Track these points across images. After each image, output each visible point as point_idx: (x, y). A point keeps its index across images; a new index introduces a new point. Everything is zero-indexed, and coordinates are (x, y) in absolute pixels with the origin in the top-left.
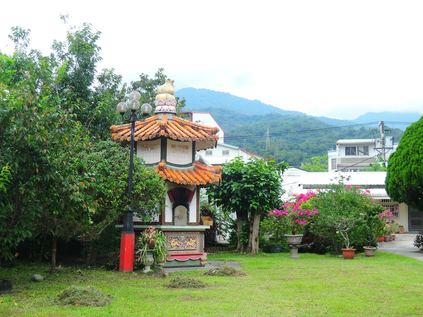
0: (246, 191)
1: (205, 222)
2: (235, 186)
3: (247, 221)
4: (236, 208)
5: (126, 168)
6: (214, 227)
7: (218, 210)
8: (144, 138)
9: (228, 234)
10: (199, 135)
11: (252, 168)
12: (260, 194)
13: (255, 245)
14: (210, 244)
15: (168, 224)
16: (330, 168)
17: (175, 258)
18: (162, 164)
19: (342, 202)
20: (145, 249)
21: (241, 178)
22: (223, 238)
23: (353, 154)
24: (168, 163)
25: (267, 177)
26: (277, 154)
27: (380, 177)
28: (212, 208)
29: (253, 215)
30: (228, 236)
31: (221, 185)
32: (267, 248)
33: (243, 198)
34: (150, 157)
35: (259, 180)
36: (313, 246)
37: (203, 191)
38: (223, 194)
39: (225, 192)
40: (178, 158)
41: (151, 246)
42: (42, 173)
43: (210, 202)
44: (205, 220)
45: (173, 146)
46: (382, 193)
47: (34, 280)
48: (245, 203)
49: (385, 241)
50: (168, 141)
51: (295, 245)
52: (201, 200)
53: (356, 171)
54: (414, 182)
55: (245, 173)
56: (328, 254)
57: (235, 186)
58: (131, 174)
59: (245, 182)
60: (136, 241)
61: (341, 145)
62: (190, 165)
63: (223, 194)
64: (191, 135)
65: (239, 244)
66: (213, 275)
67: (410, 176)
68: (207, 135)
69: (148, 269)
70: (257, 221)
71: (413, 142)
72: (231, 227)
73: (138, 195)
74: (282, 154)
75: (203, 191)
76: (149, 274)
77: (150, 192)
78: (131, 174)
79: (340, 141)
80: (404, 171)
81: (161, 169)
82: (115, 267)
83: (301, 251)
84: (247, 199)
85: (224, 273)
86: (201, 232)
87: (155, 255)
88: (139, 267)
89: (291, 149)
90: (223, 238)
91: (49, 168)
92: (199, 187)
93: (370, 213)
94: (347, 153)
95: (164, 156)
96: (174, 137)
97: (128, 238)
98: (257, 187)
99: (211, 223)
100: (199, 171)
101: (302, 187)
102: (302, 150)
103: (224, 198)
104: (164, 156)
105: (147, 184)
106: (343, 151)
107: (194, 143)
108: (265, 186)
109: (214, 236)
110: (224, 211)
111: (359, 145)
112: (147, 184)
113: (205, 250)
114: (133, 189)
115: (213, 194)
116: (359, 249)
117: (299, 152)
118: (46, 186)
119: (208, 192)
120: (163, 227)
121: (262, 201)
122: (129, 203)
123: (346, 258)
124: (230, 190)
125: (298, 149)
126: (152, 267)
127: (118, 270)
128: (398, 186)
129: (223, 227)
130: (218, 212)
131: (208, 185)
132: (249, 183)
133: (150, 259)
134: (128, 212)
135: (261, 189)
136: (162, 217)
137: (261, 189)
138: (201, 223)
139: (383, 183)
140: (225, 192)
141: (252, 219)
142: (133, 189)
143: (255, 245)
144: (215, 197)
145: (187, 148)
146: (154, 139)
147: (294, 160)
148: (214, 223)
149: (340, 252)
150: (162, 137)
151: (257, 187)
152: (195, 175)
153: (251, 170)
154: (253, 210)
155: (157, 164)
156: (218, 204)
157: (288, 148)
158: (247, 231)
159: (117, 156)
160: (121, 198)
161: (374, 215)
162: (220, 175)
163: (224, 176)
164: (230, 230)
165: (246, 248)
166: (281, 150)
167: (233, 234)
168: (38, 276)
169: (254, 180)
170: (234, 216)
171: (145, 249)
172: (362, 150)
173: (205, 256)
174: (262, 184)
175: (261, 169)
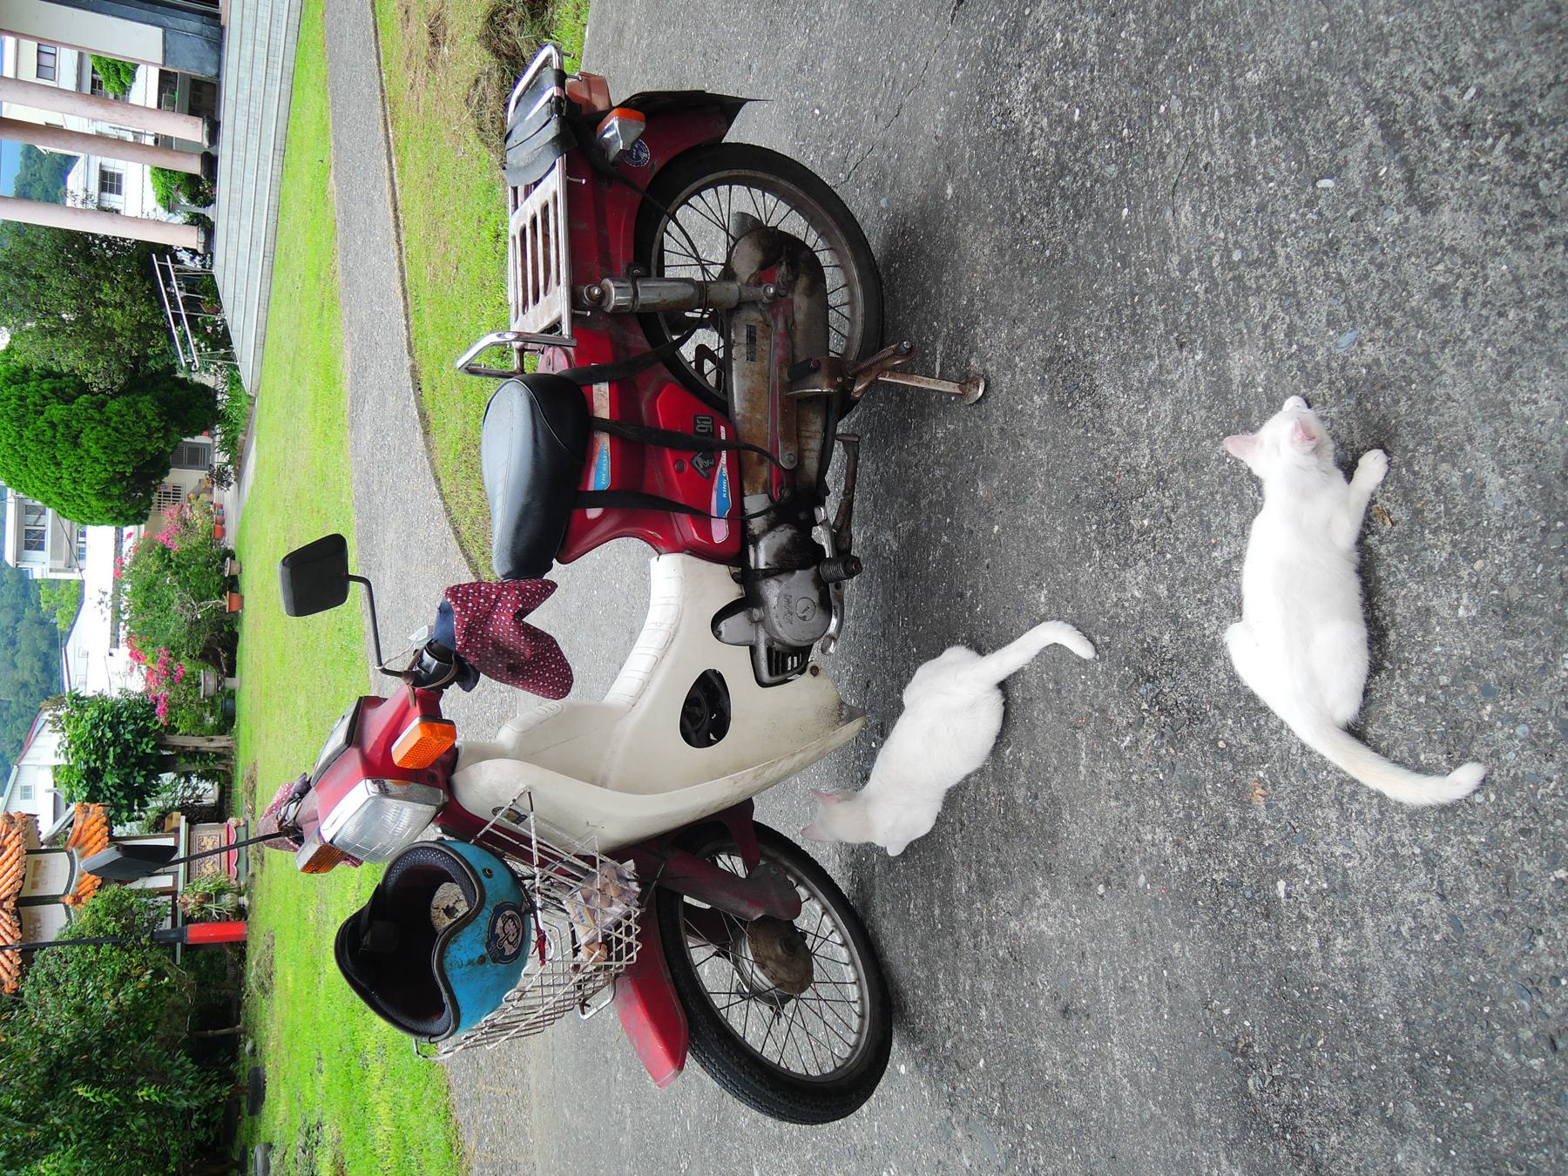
0: (120, 760)
1: (174, 825)
2: (111, 779)
3: (178, 755)
4: (153, 775)
5: (77, 950)
6: (184, 809)
7: (155, 804)
8: (18, 935)
9: (201, 785)
10: (15, 844)
11: (77, 752)
12: (128, 736)
13: (220, 742)
14: (219, 813)
15: (175, 881)
16: (74, 576)
17: (233, 865)
18: (68, 900)
19: (146, 605)
20: (212, 907)
21: (96, 769)
22: (209, 792)
23: (42, 535)
24: (67, 891)
25: (95, 726)
26: (26, 676)
27: (100, 538)
28: (151, 814)
29: (166, 748)
30: (204, 785)
31: (107, 802)
32: (228, 721)
33: (134, 765)
34: (54, 922)
35: (100, 739)
36: (225, 649)
37: (118, 831)
38: (124, 797)
39: (121, 794)
40: (57, 874)
41: (208, 898)
42: (89, 1049)
43: (140, 818)
44: (169, 824)
45: (34, 885)
46: (134, 533)
47: (253, 1050)
48: (143, 761)
49: (223, 522)
50: (23, 894)
51: (219, 683)
52: (136, 832)
53: (82, 550)
54: (115, 491)
55: (87, 762)
56: (237, 629)
57: (111, 779)
58: (89, 942)
59: (103, 763)
60: (200, 920)
61: (18, 558)
62: (70, 855)
63: (124, 797)
64: (15, 856)
65: (220, 768)
66: (254, 808)
67: (103, 495)
68: (14, 832)
69: (244, 900)
70: (177, 740)
71: (38, 484)
72: (188, 780)
73: (124, 927)
74: (27, 665)
75: (118, 831)
76: (250, 897)
77: (119, 909)
78: (89, 942)
79: (9, 557)
80: (94, 503)
81: (77, 900)
82: (240, 947)
83: (232, 672)
84: (137, 757)
85: (252, 792)
86: (190, 830)
87: (221, 892)
88: (241, 913)
89: (13, 643)
90: (209, 792)
91: (80, 1039)
92: (112, 839)
93: (168, 567)
94: (40, 547)
95: (54, 899)
96: (18, 884)
97: (194, 933)
98: (113, 743)
99: (176, 814)
100: (82, 839)
101: (114, 651)
102: (18, 621)
103: (136, 795)
104: (54, 899)
105: (107, 915)
106: (35, 554)
107: (29, 852)
108: (112, 727)
109: (204, 807)
110: (158, 793)
111: (20, 523)
112: (107, 915)
113: (225, 820)
114: (115, 934)
115: (124, 815)
116: (232, 584)
117: (22, 626)
118: (109, 1044)
119: (121, 823)
120: (180, 889)
121: (142, 733)
122: (138, 939)
123: (242, 607)
124: (119, 787)
125: (14, 629)
126: (240, 894)
127: (245, 944)
128: (120, 513)
129: (187, 794)
130: (160, 804)
131: (109, 823)
132: (105, 755)
133: (227, 899)
134: (152, 938)
135: (117, 735)
136: (164, 892)
137: (117, 735)
138: (177, 830)
139: (112, 529)
140: (121, 794)
141: (173, 748)
142: (115, 934)
143: (220, 742)
144: (131, 810)
145: (38, 863)
146: (19, 918)
147: (44, 638)
148: (178, 809)
149: (236, 613)
150: (17, 904)
151: (113, 743)
152: (90, 844)
153: (82, 753)
154: (157, 747)
155: (67, 907)
156: (143, 804)
157: (10, 651)
158: (195, 755)
159: (54, 969)
160: (129, 951)
161: (171, 560)
162: (92, 807)
163: (91, 798)
164: (194, 781)
165: (225, 755)
166: (15, 666)
167: (201, 777)
168: (249, 1046)
169: (100, 748)
170: (167, 778)
171: (212, 907)
172: (32, 518)
173: (232, 821)
174: (109, 735)
175: (79, 737)
